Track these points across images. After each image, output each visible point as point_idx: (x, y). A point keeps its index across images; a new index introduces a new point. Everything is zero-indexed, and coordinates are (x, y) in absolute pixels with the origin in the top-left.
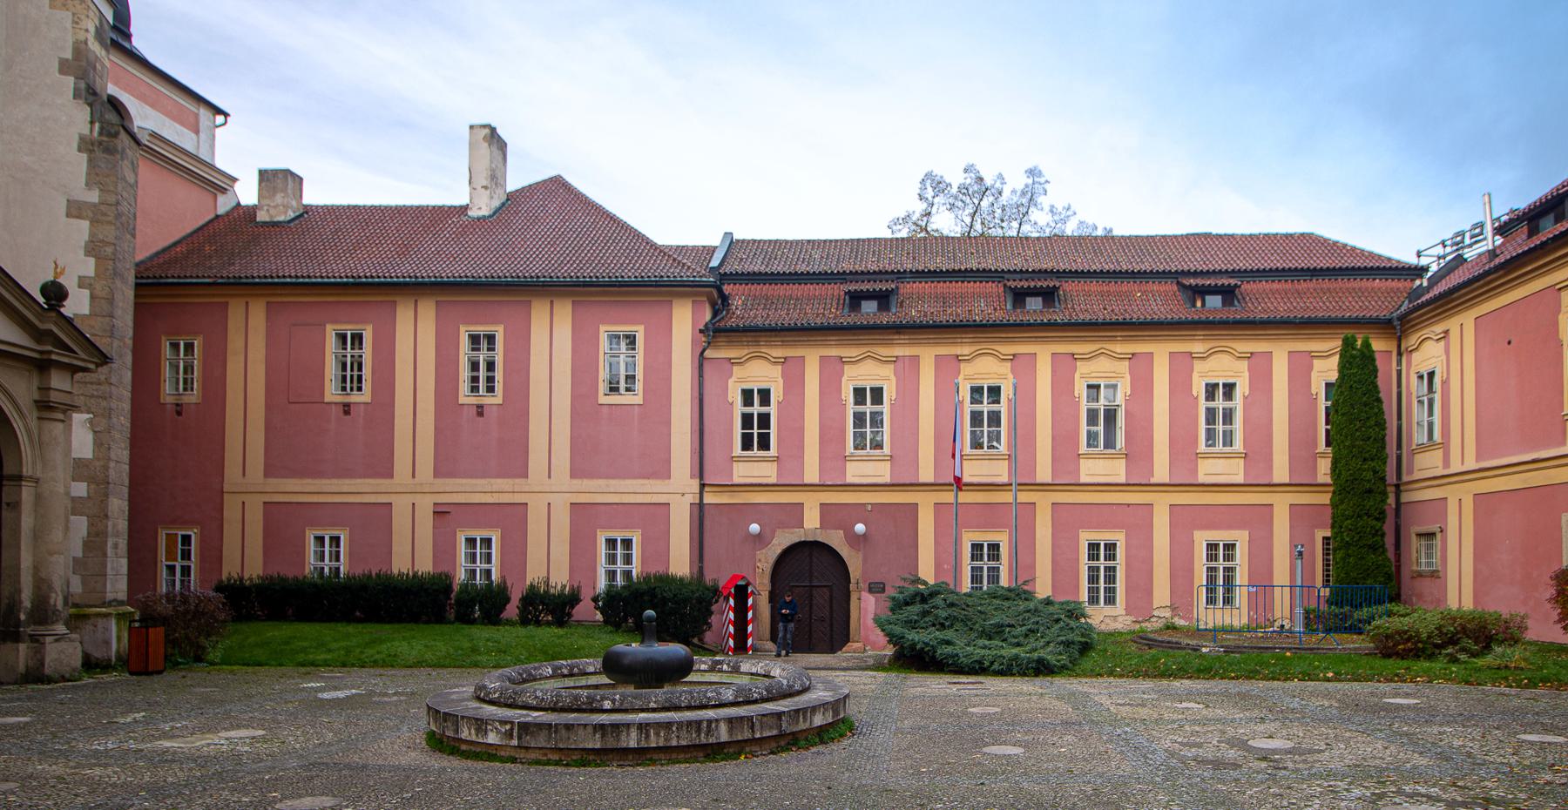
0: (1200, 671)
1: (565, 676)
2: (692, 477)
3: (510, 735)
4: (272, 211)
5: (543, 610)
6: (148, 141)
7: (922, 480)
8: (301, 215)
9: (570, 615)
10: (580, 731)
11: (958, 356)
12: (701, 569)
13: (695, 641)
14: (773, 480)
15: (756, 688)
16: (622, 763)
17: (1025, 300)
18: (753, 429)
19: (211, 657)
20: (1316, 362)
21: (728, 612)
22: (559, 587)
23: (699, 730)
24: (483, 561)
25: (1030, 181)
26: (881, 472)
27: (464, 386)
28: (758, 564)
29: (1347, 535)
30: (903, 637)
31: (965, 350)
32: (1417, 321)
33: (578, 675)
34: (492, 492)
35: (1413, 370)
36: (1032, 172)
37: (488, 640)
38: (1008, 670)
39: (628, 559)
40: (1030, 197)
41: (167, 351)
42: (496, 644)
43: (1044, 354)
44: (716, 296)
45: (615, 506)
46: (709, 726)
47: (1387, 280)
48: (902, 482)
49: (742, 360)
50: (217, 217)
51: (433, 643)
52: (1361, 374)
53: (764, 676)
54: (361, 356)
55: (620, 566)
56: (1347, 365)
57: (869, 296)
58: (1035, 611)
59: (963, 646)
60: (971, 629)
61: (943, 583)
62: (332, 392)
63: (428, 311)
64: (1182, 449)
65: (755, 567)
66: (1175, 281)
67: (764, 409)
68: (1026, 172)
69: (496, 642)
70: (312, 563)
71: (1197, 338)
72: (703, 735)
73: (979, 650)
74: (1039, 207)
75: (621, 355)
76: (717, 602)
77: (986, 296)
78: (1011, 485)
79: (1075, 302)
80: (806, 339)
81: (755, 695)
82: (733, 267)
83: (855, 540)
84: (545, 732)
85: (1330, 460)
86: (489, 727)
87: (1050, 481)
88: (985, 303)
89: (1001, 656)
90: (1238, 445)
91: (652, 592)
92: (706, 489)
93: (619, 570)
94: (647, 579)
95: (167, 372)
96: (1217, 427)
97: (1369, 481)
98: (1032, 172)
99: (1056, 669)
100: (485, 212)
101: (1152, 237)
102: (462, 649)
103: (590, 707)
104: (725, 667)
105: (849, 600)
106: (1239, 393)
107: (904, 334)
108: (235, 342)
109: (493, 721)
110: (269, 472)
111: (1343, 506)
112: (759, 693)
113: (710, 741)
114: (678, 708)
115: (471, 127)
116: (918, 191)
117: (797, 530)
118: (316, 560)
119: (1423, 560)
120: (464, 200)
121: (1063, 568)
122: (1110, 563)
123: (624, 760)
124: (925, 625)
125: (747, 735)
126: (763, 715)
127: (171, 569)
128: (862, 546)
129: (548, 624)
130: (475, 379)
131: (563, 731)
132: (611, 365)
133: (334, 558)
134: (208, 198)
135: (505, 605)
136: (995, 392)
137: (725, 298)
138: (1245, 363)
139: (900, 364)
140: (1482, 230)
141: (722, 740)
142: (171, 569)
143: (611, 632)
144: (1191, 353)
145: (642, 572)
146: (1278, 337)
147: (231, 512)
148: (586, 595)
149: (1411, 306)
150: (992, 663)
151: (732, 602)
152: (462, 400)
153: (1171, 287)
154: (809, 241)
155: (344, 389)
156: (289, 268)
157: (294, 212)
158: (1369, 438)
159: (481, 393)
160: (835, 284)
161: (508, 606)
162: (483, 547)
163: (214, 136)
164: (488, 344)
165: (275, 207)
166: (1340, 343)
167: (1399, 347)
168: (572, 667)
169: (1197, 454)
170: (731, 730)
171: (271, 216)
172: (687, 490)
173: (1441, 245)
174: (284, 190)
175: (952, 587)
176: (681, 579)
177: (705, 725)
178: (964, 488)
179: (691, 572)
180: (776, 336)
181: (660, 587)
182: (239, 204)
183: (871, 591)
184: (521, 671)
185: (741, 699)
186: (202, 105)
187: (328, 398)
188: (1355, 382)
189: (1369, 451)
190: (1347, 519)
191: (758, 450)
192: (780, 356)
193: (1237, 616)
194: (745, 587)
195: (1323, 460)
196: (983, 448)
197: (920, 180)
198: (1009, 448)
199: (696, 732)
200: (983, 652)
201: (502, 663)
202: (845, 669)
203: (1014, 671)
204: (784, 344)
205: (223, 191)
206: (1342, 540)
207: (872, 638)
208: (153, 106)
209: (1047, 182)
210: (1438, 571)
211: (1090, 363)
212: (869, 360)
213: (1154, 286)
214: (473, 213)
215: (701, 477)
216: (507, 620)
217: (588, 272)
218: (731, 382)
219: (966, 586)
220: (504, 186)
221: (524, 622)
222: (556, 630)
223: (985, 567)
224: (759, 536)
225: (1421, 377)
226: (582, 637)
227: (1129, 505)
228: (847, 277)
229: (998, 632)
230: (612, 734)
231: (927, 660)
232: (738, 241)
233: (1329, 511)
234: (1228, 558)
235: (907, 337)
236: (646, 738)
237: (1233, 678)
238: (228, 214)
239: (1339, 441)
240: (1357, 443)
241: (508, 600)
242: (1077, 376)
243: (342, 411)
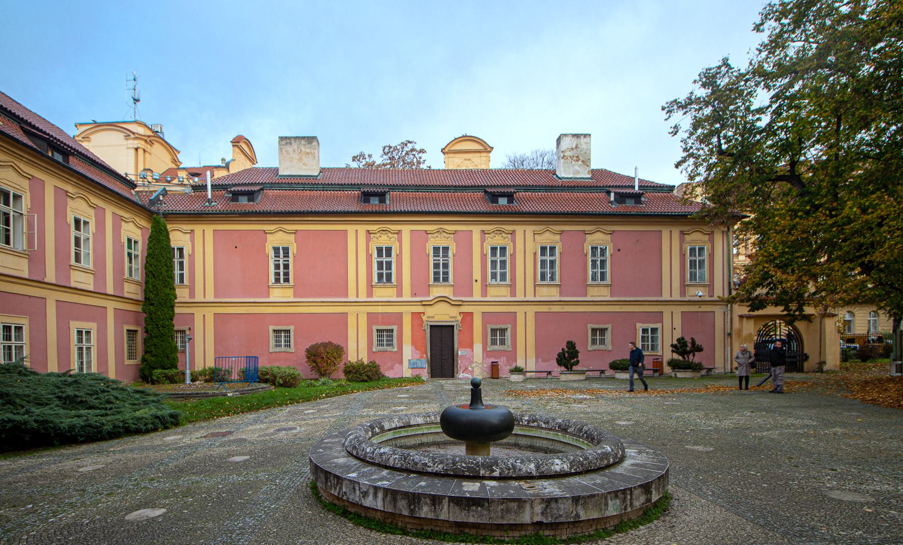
53: (404, 427)
57: (503, 195)
80: (278, 219)
90: (608, 281)
227: (30, 296)
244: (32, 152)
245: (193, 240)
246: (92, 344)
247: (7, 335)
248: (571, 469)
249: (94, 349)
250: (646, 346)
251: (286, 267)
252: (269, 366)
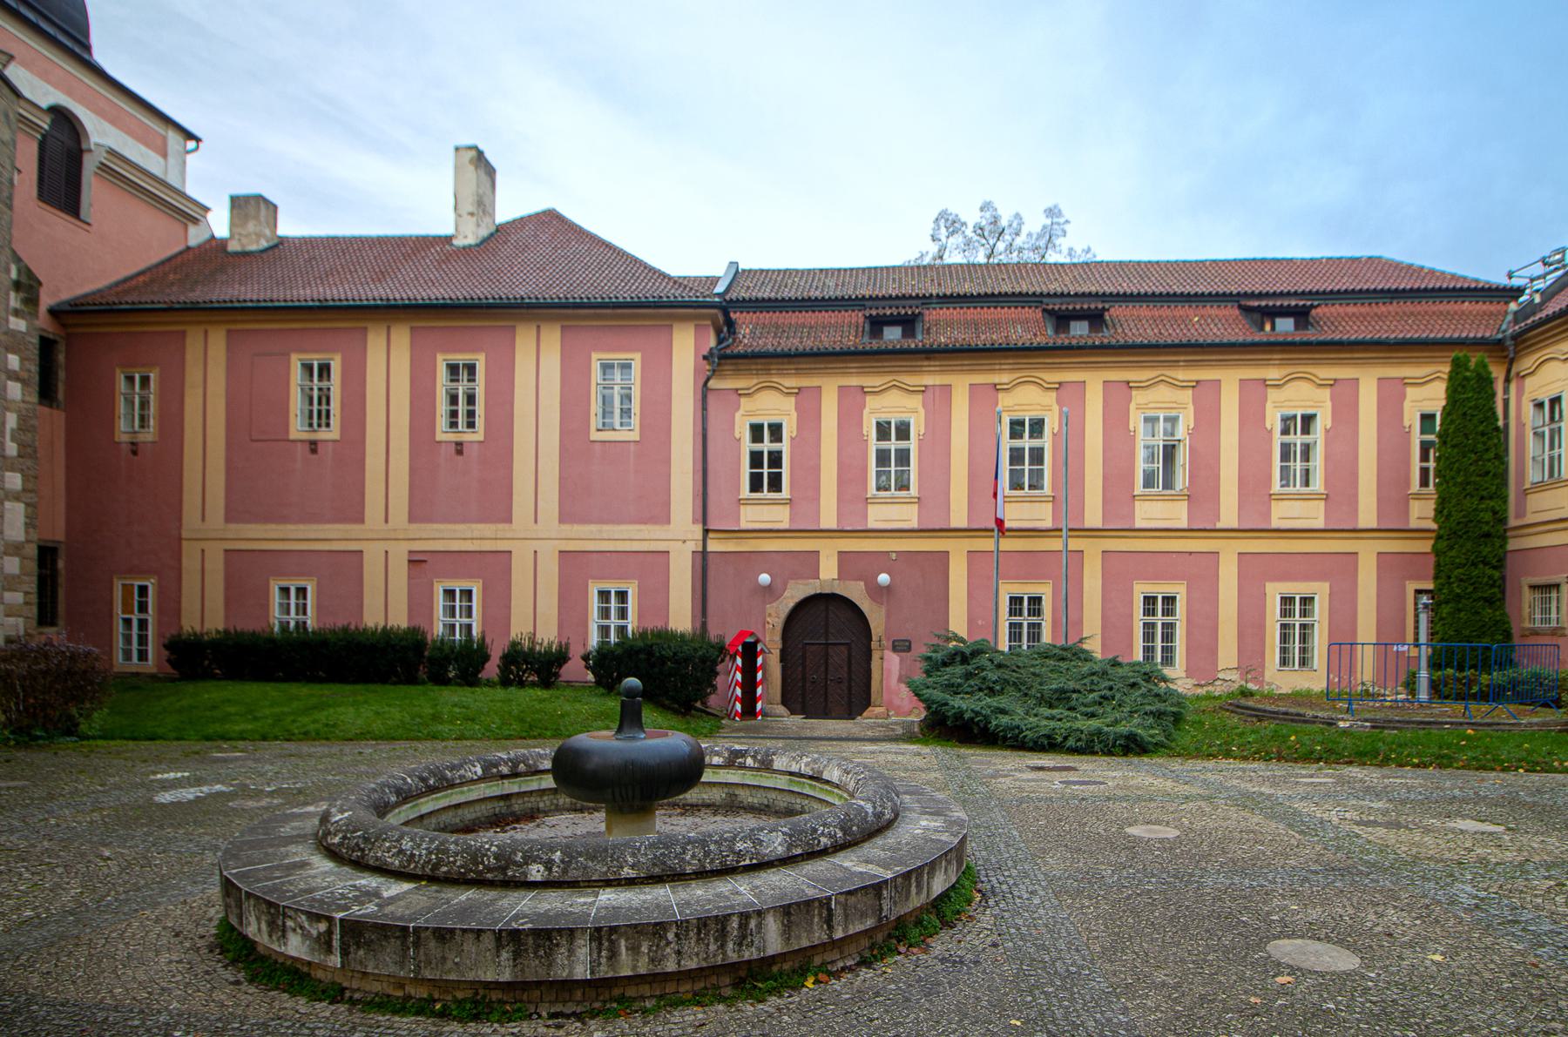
0: (1362, 754)
1: (503, 777)
3: (325, 943)
4: (244, 241)
5: (527, 668)
6: (105, 158)
7: (954, 525)
8: (276, 246)
9: (557, 675)
10: (469, 946)
11: (995, 385)
12: (704, 625)
13: (698, 705)
14: (785, 525)
15: (824, 825)
16: (558, 1008)
17: (1069, 325)
18: (762, 468)
19: (83, 727)
20: (1410, 391)
21: (735, 673)
22: (545, 643)
23: (722, 935)
24: (464, 614)
25: (1048, 222)
26: (908, 516)
27: (442, 422)
28: (768, 619)
29: (1458, 586)
30: (946, 704)
31: (1003, 378)
32: (1533, 341)
33: (525, 774)
34: (472, 539)
36: (1051, 212)
37: (455, 705)
38: (1090, 746)
39: (623, 614)
40: (1049, 237)
41: (122, 385)
42: (464, 710)
43: (1094, 382)
44: (721, 322)
45: (608, 554)
46: (743, 926)
47: (1477, 302)
48: (931, 526)
49: (750, 391)
50: (189, 248)
51: (387, 709)
52: (1477, 399)
53: (811, 778)
54: (329, 389)
55: (614, 621)
56: (1459, 389)
58: (1103, 674)
59: (1016, 713)
60: (1026, 695)
61: (983, 640)
62: (297, 428)
63: (401, 337)
64: (1254, 488)
65: (765, 623)
66: (1236, 304)
67: (775, 446)
68: (1045, 211)
69: (464, 707)
70: (278, 616)
71: (1271, 362)
72: (730, 945)
73: (1041, 721)
74: (1058, 249)
75: (616, 387)
76: (723, 661)
77: (1024, 322)
78: (1061, 530)
79: (1125, 326)
81: (824, 840)
82: (740, 293)
83: (877, 592)
84: (394, 944)
85: (1433, 501)
86: (290, 923)
87: (1100, 525)
88: (1024, 327)
89: (1078, 730)
90: (1318, 484)
91: (648, 650)
92: (711, 535)
93: (612, 626)
94: (643, 635)
95: (122, 407)
96: (1292, 464)
97: (1487, 523)
98: (1051, 212)
99: (1151, 747)
100: (471, 241)
101: (1201, 262)
102: (421, 717)
103: (501, 877)
104: (749, 761)
105: (871, 659)
106: (1320, 426)
107: (935, 359)
108: (193, 374)
109: (297, 910)
110: (231, 516)
111: (1453, 553)
112: (830, 836)
113: (747, 956)
114: (675, 877)
115: (457, 149)
116: (931, 232)
117: (812, 581)
118: (282, 613)
119: (1538, 616)
120: (448, 230)
121: (1114, 623)
122: (1169, 619)
123: (565, 1002)
124: (969, 690)
125: (819, 935)
126: (850, 893)
127: (128, 622)
128: (885, 598)
129: (533, 684)
130: (454, 414)
131: (432, 944)
132: (604, 397)
133: (301, 611)
134: (178, 228)
135: (484, 663)
136: (1037, 427)
137: (730, 324)
138: (1327, 392)
139: (929, 393)
140: (1564, 256)
141: (770, 951)
142: (128, 622)
143: (603, 694)
144: (1265, 380)
145: (638, 627)
147: (190, 562)
148: (576, 652)
149: (1517, 327)
150: (1066, 738)
151: (739, 661)
152: (440, 437)
153: (1232, 311)
154: (821, 270)
155: (311, 425)
156: (250, 292)
157: (268, 241)
158: (1487, 473)
159: (460, 429)
160: (853, 311)
161: (487, 665)
162: (464, 599)
163: (184, 162)
164: (469, 375)
165: (246, 236)
166: (1447, 369)
167: (1509, 371)
168: (515, 763)
169: (1271, 495)
170: (787, 932)
171: (243, 245)
172: (690, 537)
173: (1540, 263)
174: (257, 218)
175: (992, 644)
176: (682, 635)
177: (735, 925)
178: (1007, 534)
179: (693, 628)
180: (789, 363)
181: (658, 644)
182: (213, 237)
183: (895, 649)
184: (425, 775)
185: (799, 851)
186: (170, 126)
187: (293, 435)
188: (1470, 408)
189: (1487, 489)
190: (1458, 568)
191: (769, 491)
192: (794, 385)
193: (1314, 680)
194: (755, 644)
195: (1417, 502)
196: (1023, 489)
197: (934, 219)
198: (1054, 489)
199: (716, 940)
200: (1052, 724)
201: (467, 734)
202: (873, 740)
203: (1096, 749)
204: (799, 372)
205: (195, 221)
206: (1451, 591)
207: (897, 702)
208: (113, 122)
209: (1067, 222)
210: (1564, 628)
211: (1147, 392)
212: (895, 391)
213: (1212, 310)
214: (458, 242)
215: (705, 522)
216: (488, 680)
217: (580, 293)
218: (738, 415)
219: (1004, 645)
220: (492, 215)
221: (505, 682)
222: (540, 693)
224: (769, 589)
225: (1540, 405)
226: (568, 701)
227: (1191, 553)
228: (866, 303)
229: (1061, 697)
230: (535, 953)
231: (975, 731)
232: (744, 271)
233: (1432, 560)
235: (937, 363)
236: (610, 958)
237: (1417, 766)
238: (200, 246)
239: (1447, 478)
240: (1473, 479)
241: (486, 658)
242: (1132, 406)
243: (308, 449)
244: (1183, 350)
247: (1034, 609)
249: (1180, 627)
250: (1291, 649)
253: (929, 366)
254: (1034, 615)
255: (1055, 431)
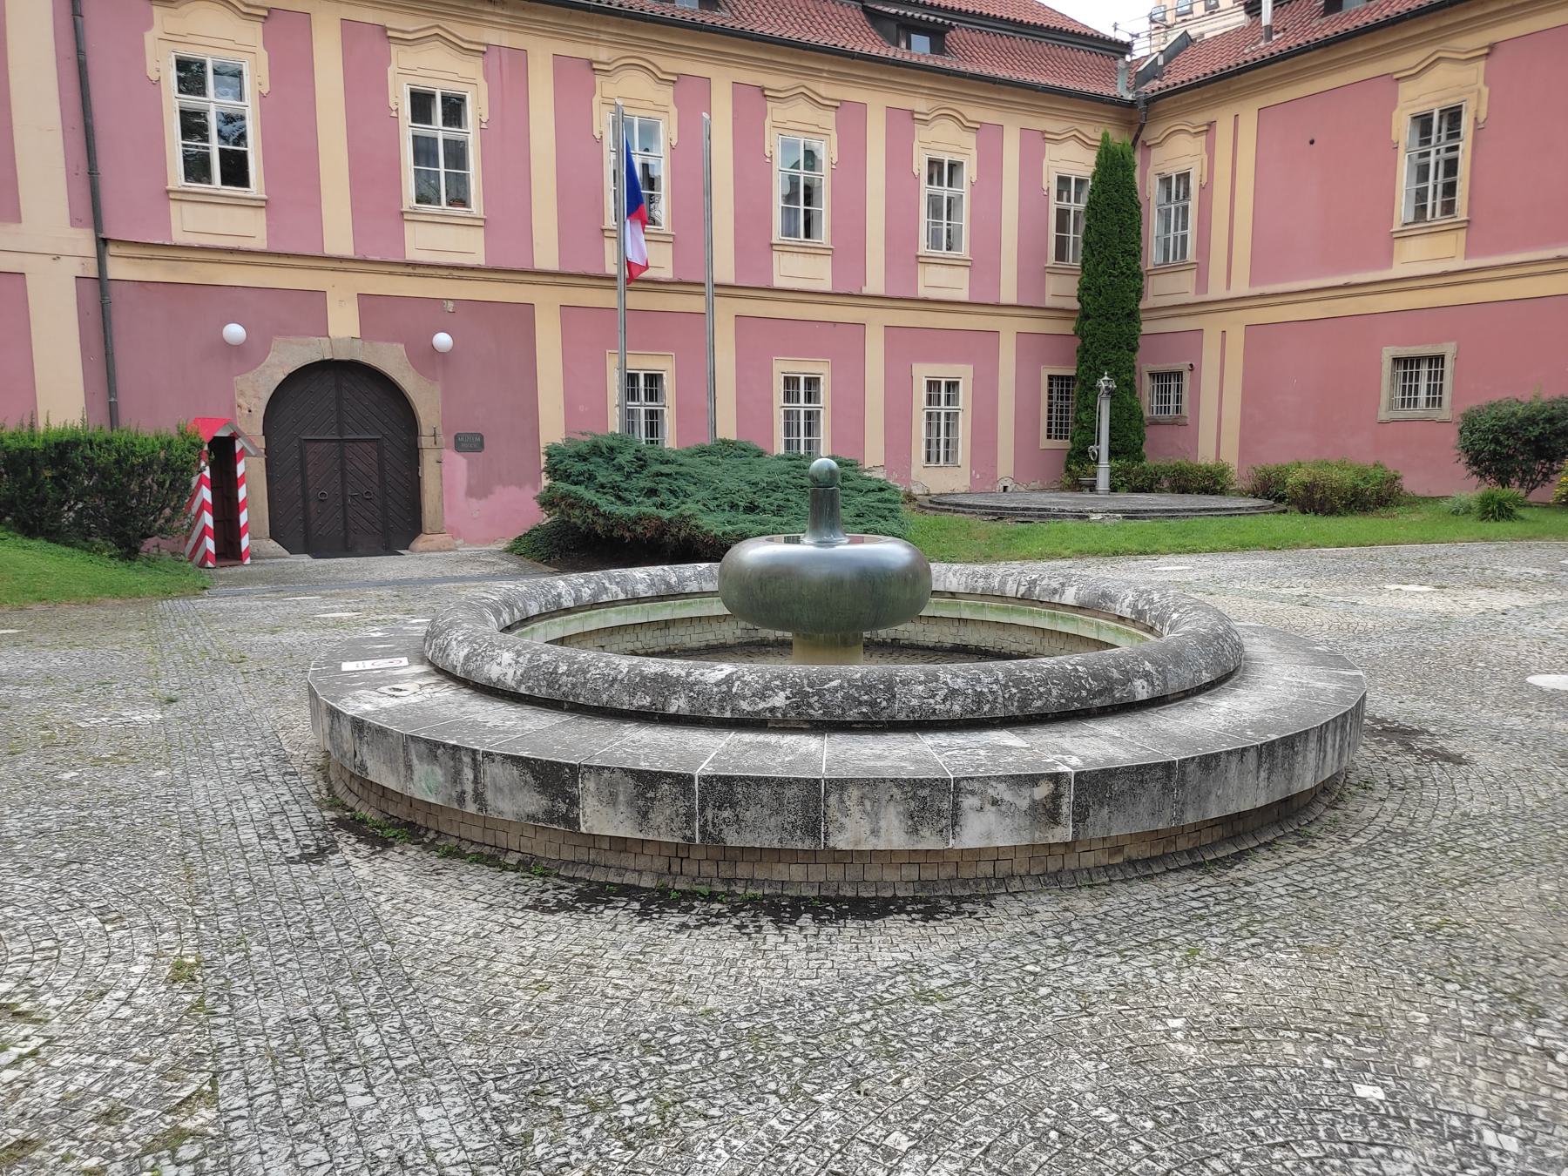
2: (75, 222)
28: (241, 401)
31: (602, 54)
35: (1151, 171)
85: (1078, 278)
87: (731, 281)
92: (112, 249)
121: (751, 405)
144: (912, 112)
146: (722, 58)
172: (68, 250)
191: (225, 181)
194: (231, 440)
211: (784, 106)
212: (801, 101)
215: (97, 223)
218: (149, 37)
223: (943, 412)
234: (652, 395)
245: (1210, 149)
246: (960, 407)
248: (520, 683)
250: (795, 443)
251: (1451, 167)
252: (1366, 460)
253: (502, 15)
254: (651, 400)
255: (674, 144)
